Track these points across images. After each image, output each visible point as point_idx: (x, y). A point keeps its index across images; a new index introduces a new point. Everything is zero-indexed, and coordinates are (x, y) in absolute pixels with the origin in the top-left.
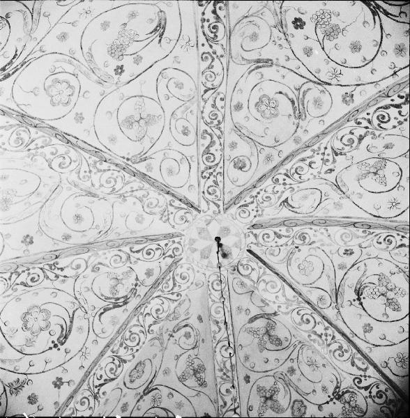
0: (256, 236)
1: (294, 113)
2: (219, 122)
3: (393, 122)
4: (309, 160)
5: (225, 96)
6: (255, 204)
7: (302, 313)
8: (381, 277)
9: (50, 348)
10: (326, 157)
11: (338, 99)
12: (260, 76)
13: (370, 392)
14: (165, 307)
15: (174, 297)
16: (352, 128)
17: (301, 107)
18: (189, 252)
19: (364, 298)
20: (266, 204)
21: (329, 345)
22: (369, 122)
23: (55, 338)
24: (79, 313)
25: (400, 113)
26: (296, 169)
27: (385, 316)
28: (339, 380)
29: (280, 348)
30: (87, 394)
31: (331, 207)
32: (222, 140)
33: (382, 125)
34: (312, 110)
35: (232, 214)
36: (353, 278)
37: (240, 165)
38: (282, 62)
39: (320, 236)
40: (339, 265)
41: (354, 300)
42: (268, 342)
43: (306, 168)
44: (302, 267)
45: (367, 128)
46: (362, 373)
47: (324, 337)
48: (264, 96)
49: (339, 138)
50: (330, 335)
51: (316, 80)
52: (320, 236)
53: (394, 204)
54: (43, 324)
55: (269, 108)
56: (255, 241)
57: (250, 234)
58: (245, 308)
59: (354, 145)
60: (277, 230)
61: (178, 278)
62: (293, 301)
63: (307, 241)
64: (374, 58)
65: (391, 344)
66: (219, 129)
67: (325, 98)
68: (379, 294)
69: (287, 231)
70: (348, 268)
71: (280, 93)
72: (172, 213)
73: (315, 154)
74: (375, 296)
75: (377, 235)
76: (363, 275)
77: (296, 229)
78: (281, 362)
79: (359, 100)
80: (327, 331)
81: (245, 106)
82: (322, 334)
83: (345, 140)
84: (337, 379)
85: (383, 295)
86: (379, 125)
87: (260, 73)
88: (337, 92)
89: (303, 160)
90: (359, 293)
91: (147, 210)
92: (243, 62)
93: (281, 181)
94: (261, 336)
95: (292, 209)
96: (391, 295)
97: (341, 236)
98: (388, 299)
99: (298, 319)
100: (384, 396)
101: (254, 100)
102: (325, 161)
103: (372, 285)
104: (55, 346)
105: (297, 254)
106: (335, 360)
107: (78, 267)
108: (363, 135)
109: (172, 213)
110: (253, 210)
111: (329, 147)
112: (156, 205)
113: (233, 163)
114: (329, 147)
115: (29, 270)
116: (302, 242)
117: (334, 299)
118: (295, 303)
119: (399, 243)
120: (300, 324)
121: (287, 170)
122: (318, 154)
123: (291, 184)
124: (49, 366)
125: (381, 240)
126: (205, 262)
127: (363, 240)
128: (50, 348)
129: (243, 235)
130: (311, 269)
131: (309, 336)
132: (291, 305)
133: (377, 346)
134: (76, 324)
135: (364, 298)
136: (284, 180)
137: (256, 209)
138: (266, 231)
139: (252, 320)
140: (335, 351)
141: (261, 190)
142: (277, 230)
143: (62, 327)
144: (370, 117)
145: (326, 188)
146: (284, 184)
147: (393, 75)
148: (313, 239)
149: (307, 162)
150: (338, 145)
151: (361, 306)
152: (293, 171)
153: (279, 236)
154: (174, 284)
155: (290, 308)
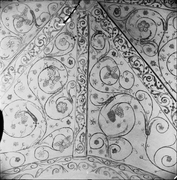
0: (84, 18)
1: (143, 39)
2: (146, 3)
3: (147, 83)
4: (126, 46)
5: (159, 8)
7: (44, 40)
8: (59, 77)
10: (128, 54)
11: (153, 59)
12: (159, 24)
13: (7, 75)
16: (144, 65)
17: (146, 42)
19: (48, 70)
20: (103, 24)
21: (28, 54)
22: (147, 73)
25: (153, 85)
26: (121, 40)
27: (40, 80)
28: (6, 59)
29: (16, 27)
31: (93, 54)
32: (136, 4)
33: (145, 78)
34: (146, 47)
35: (97, 6)
36: (58, 65)
37: (117, 11)
38: (166, 35)
39: (83, 49)
40: (63, 58)
41: (47, 65)
42: (18, 21)
43: (122, 44)
44: (64, 40)
45: (144, 71)
46: (16, 71)
47: (32, 51)
48: (149, 25)
49: (138, 60)
50: (34, 54)
51: (159, 49)
52: (83, 49)
53: (95, 82)
55: (143, 27)
56: (81, 17)
57: (85, 15)
58: (40, 9)
59: (134, 66)
60: (87, 28)
62: (50, 35)
63: (81, 43)
64: (173, 75)
65: (29, 83)
66: (142, 3)
67: (152, 54)
68: (50, 77)
69: (86, 34)
70: (62, 62)
71: (151, 33)
73: (129, 49)
74: (49, 75)
75: (85, 75)
76: (58, 69)
77: (87, 38)
78: (7, 27)
79: (154, 68)
80: (36, 53)
81: (145, 16)
82: (34, 50)
83: (137, 62)
84: (7, 57)
85: (50, 78)
86: (146, 77)
87: (161, 24)
88: (155, 58)
89: (126, 43)
90: (50, 67)
92: (168, 17)
93: (114, 32)
94: (22, 17)
95: (93, 36)
96: (50, 82)
97: (83, 59)
98: (48, 81)
99: (41, 38)
100: (6, 82)
101: (148, 21)
102: (125, 53)
103: (54, 73)
105: (70, 38)
106: (22, 56)
108: (140, 70)
110: (99, 17)
111: (133, 55)
113: (118, 7)
114: (133, 55)
116: (80, 41)
117: (48, 56)
118: (49, 37)
119: (82, 85)
120: (38, 39)
121: (121, 35)
122: (129, 50)
123: (113, 36)
125: (82, 77)
127: (82, 70)
129: (84, 10)
130: (62, 44)
131: (32, 43)
132: (48, 34)
133: (27, 77)
135: (48, 70)
136: (115, 34)
138: (86, 23)
139: (32, 12)
140: (26, 57)
141: (110, 22)
142: (87, 28)
144: (150, 73)
145: (103, 52)
146: (113, 33)
147: (166, 82)
148: (82, 46)
149: (125, 45)
150: (134, 59)
151: (44, 68)
152: (120, 38)
153: (83, 29)
155: (46, 34)
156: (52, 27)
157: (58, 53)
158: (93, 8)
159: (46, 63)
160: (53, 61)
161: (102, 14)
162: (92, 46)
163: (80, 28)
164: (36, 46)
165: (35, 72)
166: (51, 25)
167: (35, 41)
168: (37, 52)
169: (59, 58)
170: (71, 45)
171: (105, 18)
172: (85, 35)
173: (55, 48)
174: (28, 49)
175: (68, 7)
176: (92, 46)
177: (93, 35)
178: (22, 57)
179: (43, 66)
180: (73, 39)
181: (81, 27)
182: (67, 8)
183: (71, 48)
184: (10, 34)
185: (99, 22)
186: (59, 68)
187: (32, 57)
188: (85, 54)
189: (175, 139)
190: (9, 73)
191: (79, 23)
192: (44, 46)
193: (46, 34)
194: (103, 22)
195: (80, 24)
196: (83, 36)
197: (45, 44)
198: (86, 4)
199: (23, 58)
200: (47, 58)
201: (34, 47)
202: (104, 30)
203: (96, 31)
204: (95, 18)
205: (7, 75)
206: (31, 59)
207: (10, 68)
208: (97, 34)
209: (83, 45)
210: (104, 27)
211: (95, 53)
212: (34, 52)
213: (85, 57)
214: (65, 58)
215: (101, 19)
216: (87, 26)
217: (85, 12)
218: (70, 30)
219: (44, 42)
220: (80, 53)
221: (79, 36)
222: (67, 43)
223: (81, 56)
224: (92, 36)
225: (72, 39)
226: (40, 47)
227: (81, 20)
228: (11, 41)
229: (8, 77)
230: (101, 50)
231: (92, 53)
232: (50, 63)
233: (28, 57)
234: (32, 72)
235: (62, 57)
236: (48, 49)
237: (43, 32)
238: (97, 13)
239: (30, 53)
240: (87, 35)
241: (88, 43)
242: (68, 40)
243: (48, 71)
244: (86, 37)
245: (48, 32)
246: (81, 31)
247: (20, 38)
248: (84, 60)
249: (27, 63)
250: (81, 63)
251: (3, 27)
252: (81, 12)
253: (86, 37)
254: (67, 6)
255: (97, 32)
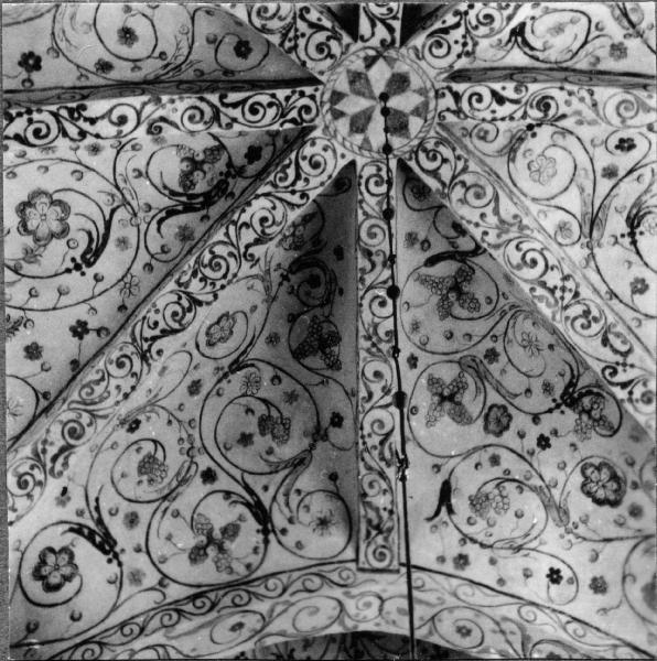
0: (457, 97)
6: (461, 30)
7: (525, 247)
9: (68, 271)
14: (278, 214)
15: (296, 199)
18: (329, 117)
19: (641, 233)
20: (483, 30)
21: (566, 308)
23: (77, 254)
24: (122, 214)
29: (476, 315)
30: (130, 350)
36: (628, 192)
40: (604, 169)
41: (623, 236)
44: (535, 166)
47: (558, 294)
50: (570, 290)
54: (56, 227)
56: (454, 107)
57: (446, 92)
61: (305, 165)
62: (512, 225)
63: (552, 112)
72: (303, 35)
76: (646, 191)
78: (475, 339)
82: (556, 287)
90: (634, 222)
91: (258, 22)
94: (445, 292)
95: (530, 53)
97: (618, 108)
104: (78, 267)
105: (530, 143)
106: (571, 332)
107: (123, 120)
109: (303, 35)
110: (456, 42)
112: (275, 15)
115: (29, 112)
117: (586, 230)
118: (515, 229)
120: (519, 267)
124: (65, 300)
126: (358, 138)
128: (68, 271)
129: (432, 94)
130: (551, 171)
131: (532, 289)
132: (507, 232)
134: (115, 233)
135: (641, 233)
137: (461, 41)
142: (497, 86)
143: (89, 234)
148: (563, 109)
151: (632, 247)
153: (500, 100)
154: (298, 177)
155: (505, 237)
156: (483, 216)
157: (582, 190)
158: (423, 64)
159: (613, 240)
160: (612, 209)
161: (445, 31)
162: (572, 58)
163: (494, 112)
164: (542, 279)
165: (639, 286)
166: (476, 218)
167: (526, 281)
168: (566, 278)
169: (605, 185)
170: (559, 140)
171: (463, 22)
172: (523, 94)
173: (560, 201)
174: (548, 305)
175: (416, 153)
176: (572, 58)
177: (525, 53)
178: (575, 331)
179: (621, 252)
180: (536, 129)
181: (491, 109)
182: (422, 156)
183: (571, 142)
184: (496, 337)
185: (475, 44)
186: (643, 187)
187: (581, 297)
188: (596, 97)
189: (445, 635)
190: (624, 385)
191: (476, 113)
192: (545, 252)
193: (505, 237)
194: (476, 28)
195: (479, 110)
196: (524, 101)
197: (538, 246)
198: (408, 85)
199: (579, 328)
200: (595, 234)
201: (543, 285)
202: (508, 24)
203: (510, 45)
204: (459, 56)
205: (631, 393)
206: (587, 302)
207: (609, 378)
208: (526, 43)
209: (561, 103)
210: (496, 25)
211: (600, 47)
212: (563, 289)
213: (608, 95)
214: (605, 164)
215: (464, 37)
216: (489, 87)
217: (437, 92)
218: (502, 141)
219: (534, 250)
220: (589, 114)
221: (525, 115)
222: (549, 153)
223: (601, 112)
224: (532, 57)
225: (534, 135)
226: (547, 266)
227: (465, 105)
228: (519, 338)
229: (638, 391)
230: (590, 21)
231: (598, 59)
232: (616, 224)
233: (577, 310)
234: (637, 297)
235: (599, 173)
236: (562, 227)
237: (497, 247)
238: (443, 51)
239: (566, 302)
240: (523, 89)
241: (554, 85)
242: (538, 150)
243: (647, 234)
244: (530, 92)
245: (497, 231)
246: (507, 109)
247: (513, 311)
248: (623, 102)
249: (596, 320)
250: (632, 118)
251: (473, 352)
252: (437, 105)
253: (530, 92)
254: (413, 156)
255: (516, 41)
